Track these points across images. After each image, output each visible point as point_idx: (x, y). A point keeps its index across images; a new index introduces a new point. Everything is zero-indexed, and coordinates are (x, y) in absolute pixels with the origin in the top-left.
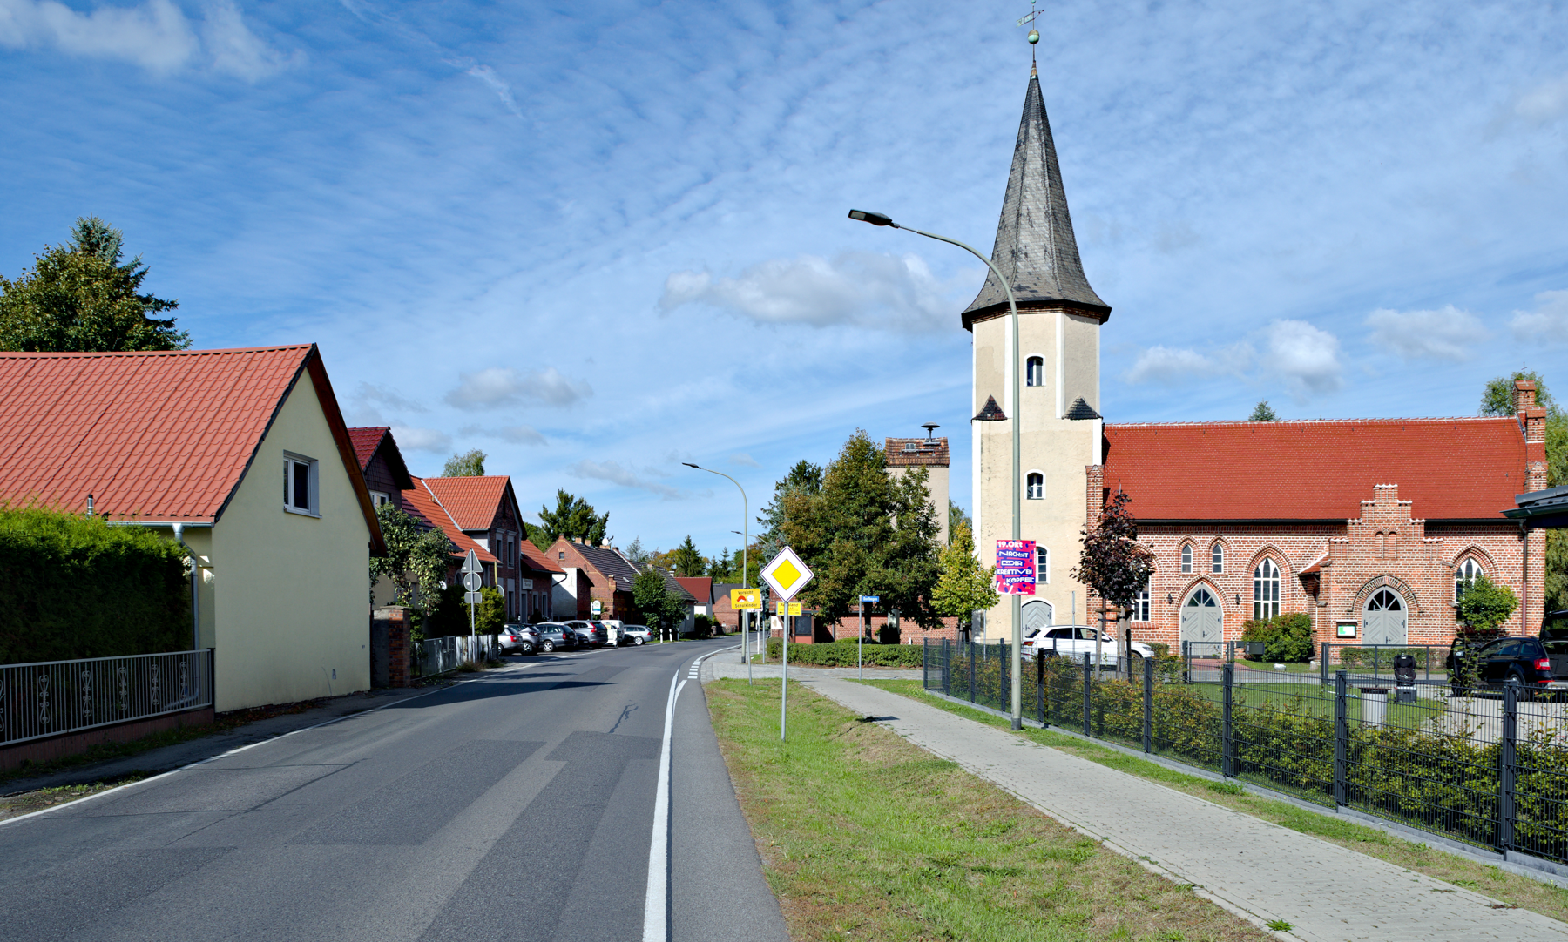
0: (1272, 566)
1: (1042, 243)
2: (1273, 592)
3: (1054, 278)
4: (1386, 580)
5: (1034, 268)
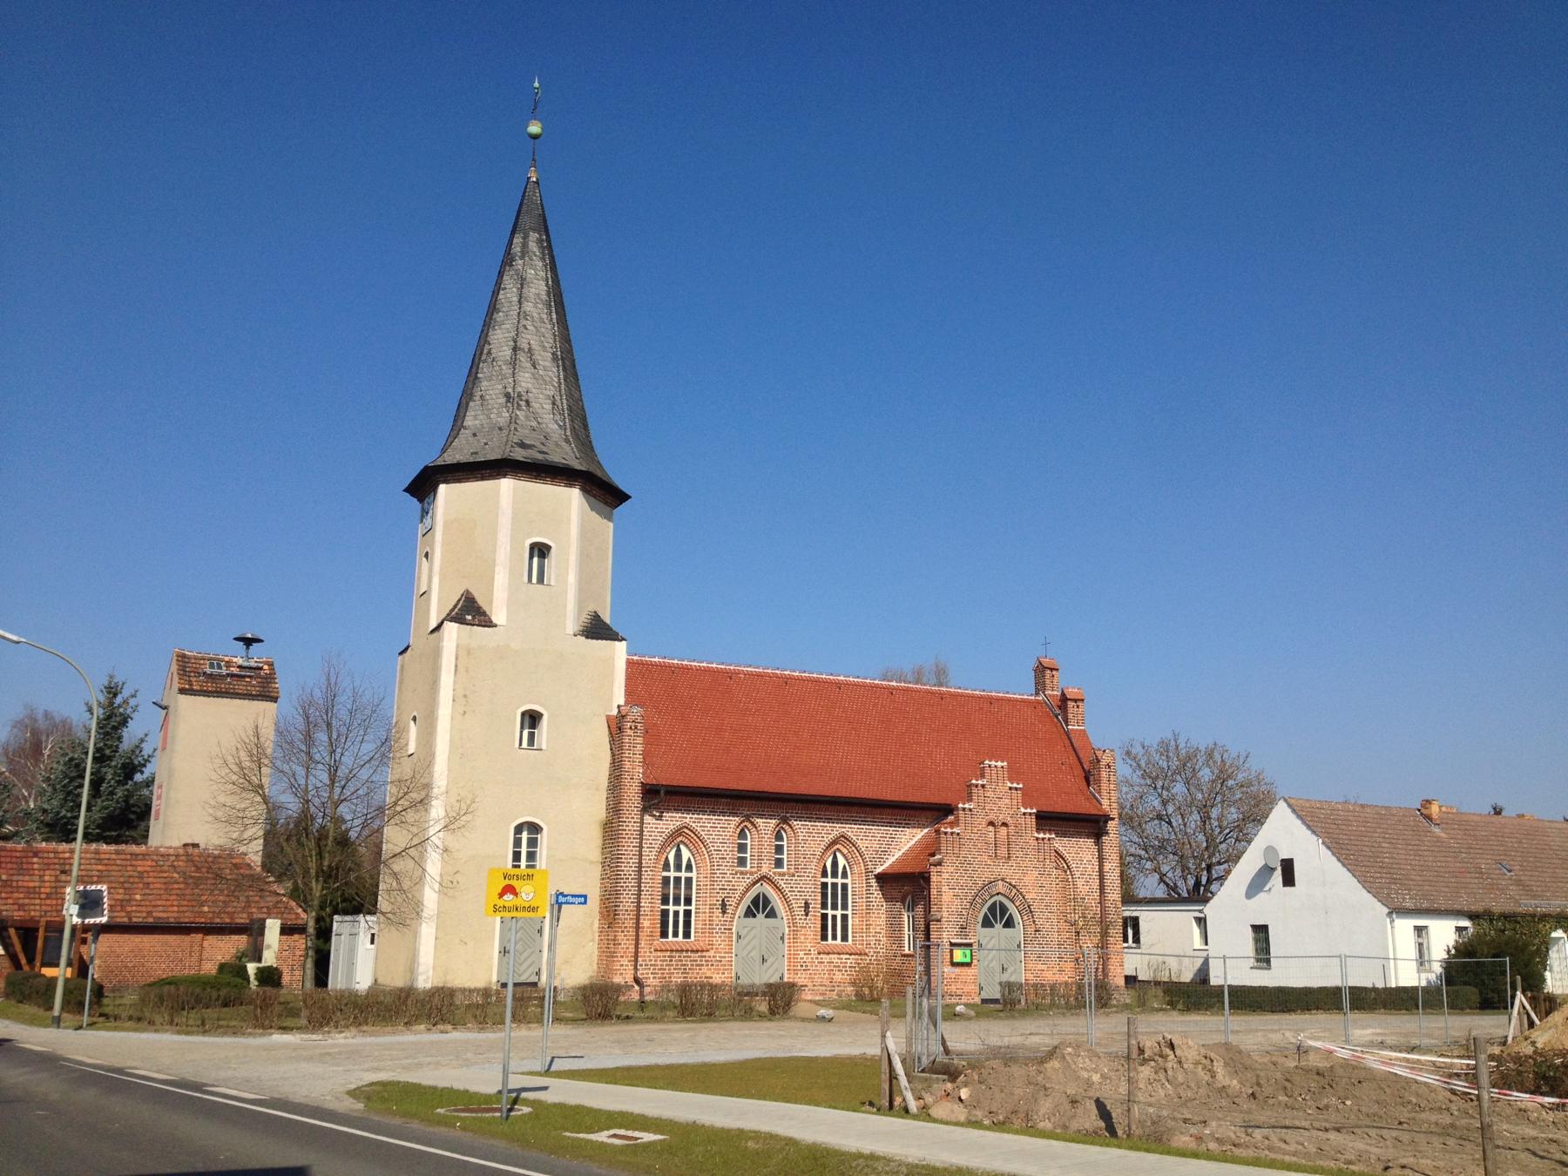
0: (841, 861)
1: (548, 393)
3: (567, 441)
4: (1000, 887)
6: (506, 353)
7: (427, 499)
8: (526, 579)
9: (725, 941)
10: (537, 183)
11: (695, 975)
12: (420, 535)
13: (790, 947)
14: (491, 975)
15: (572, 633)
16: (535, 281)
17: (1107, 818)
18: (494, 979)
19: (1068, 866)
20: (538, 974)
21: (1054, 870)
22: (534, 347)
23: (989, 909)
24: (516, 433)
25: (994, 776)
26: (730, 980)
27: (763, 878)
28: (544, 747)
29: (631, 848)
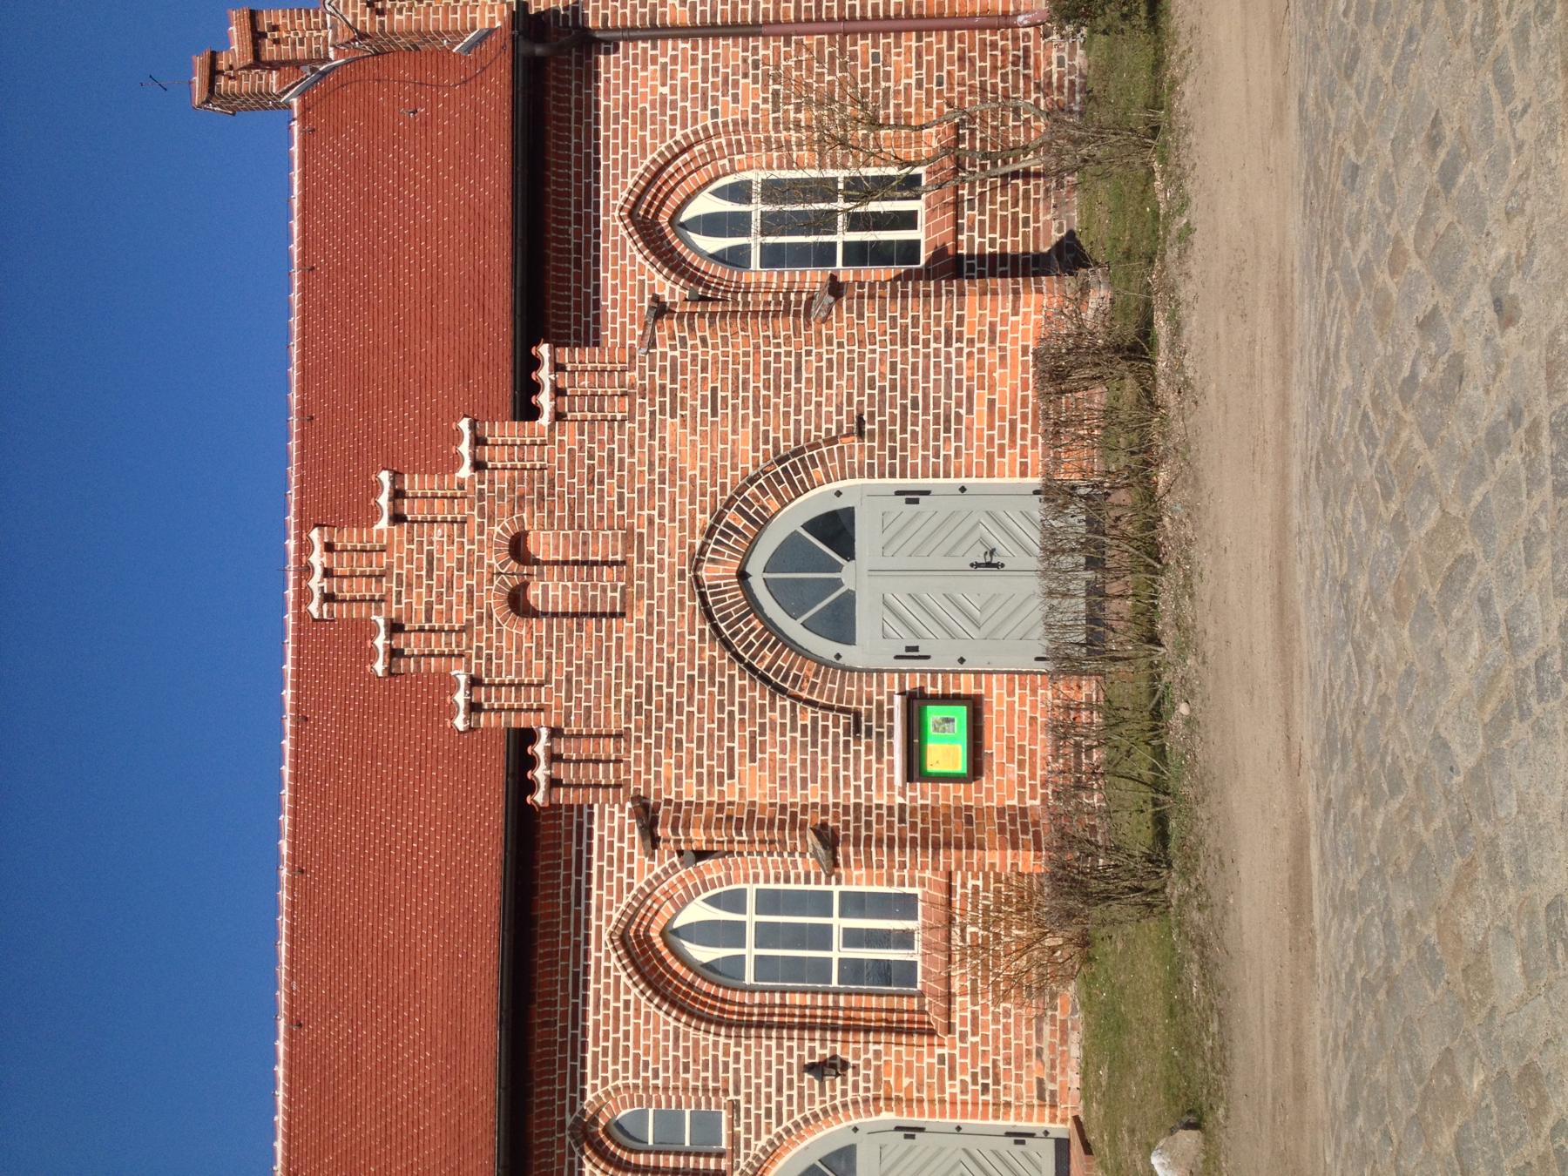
4: (717, 572)
19: (683, 151)
21: (659, 350)
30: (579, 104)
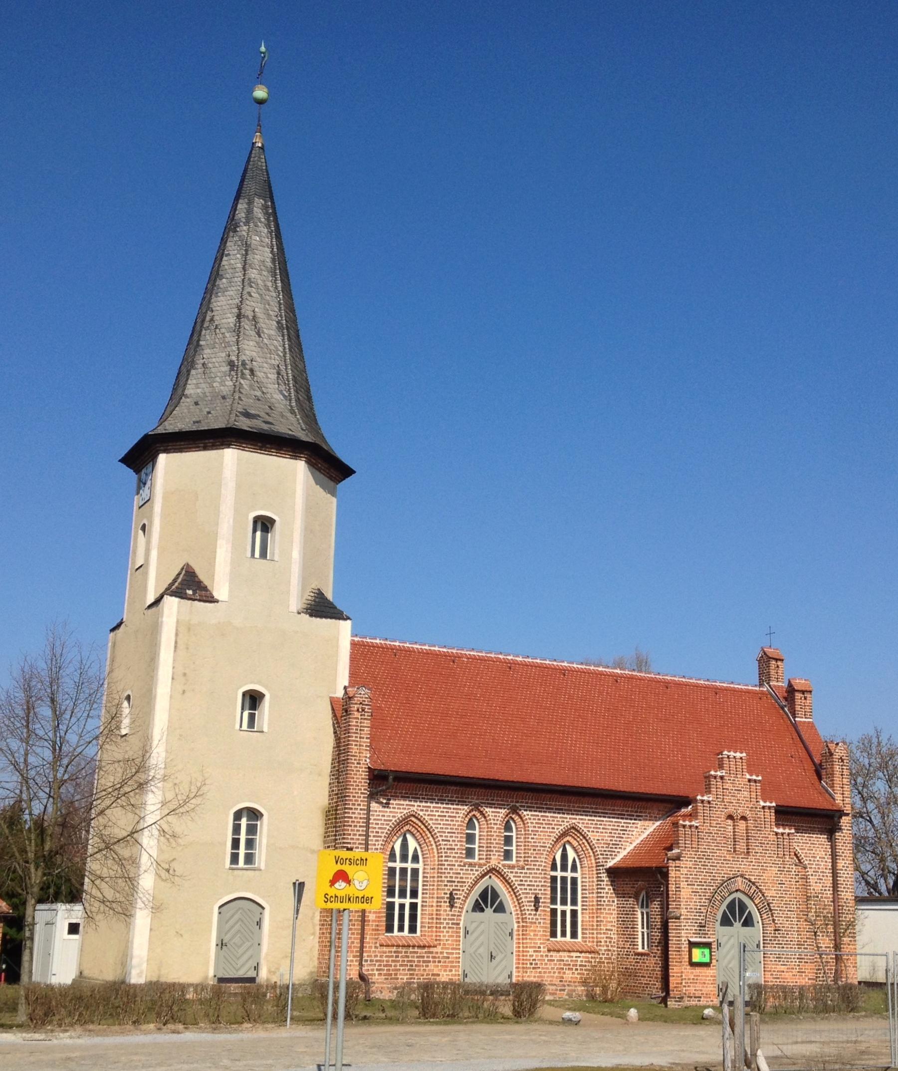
0: (571, 855)
1: (273, 362)
2: (571, 894)
3: (292, 412)
4: (740, 883)
5: (263, 393)
6: (229, 320)
7: (144, 471)
8: (249, 554)
9: (452, 936)
10: (262, 148)
11: (422, 973)
12: (135, 508)
13: (519, 943)
14: (208, 970)
15: (295, 611)
16: (260, 248)
17: (841, 813)
18: (211, 973)
20: (256, 968)
21: (794, 867)
22: (258, 315)
23: (728, 907)
24: (240, 402)
25: (733, 767)
26: (457, 978)
27: (493, 871)
28: (265, 729)
29: (357, 837)
30: (815, 827)
